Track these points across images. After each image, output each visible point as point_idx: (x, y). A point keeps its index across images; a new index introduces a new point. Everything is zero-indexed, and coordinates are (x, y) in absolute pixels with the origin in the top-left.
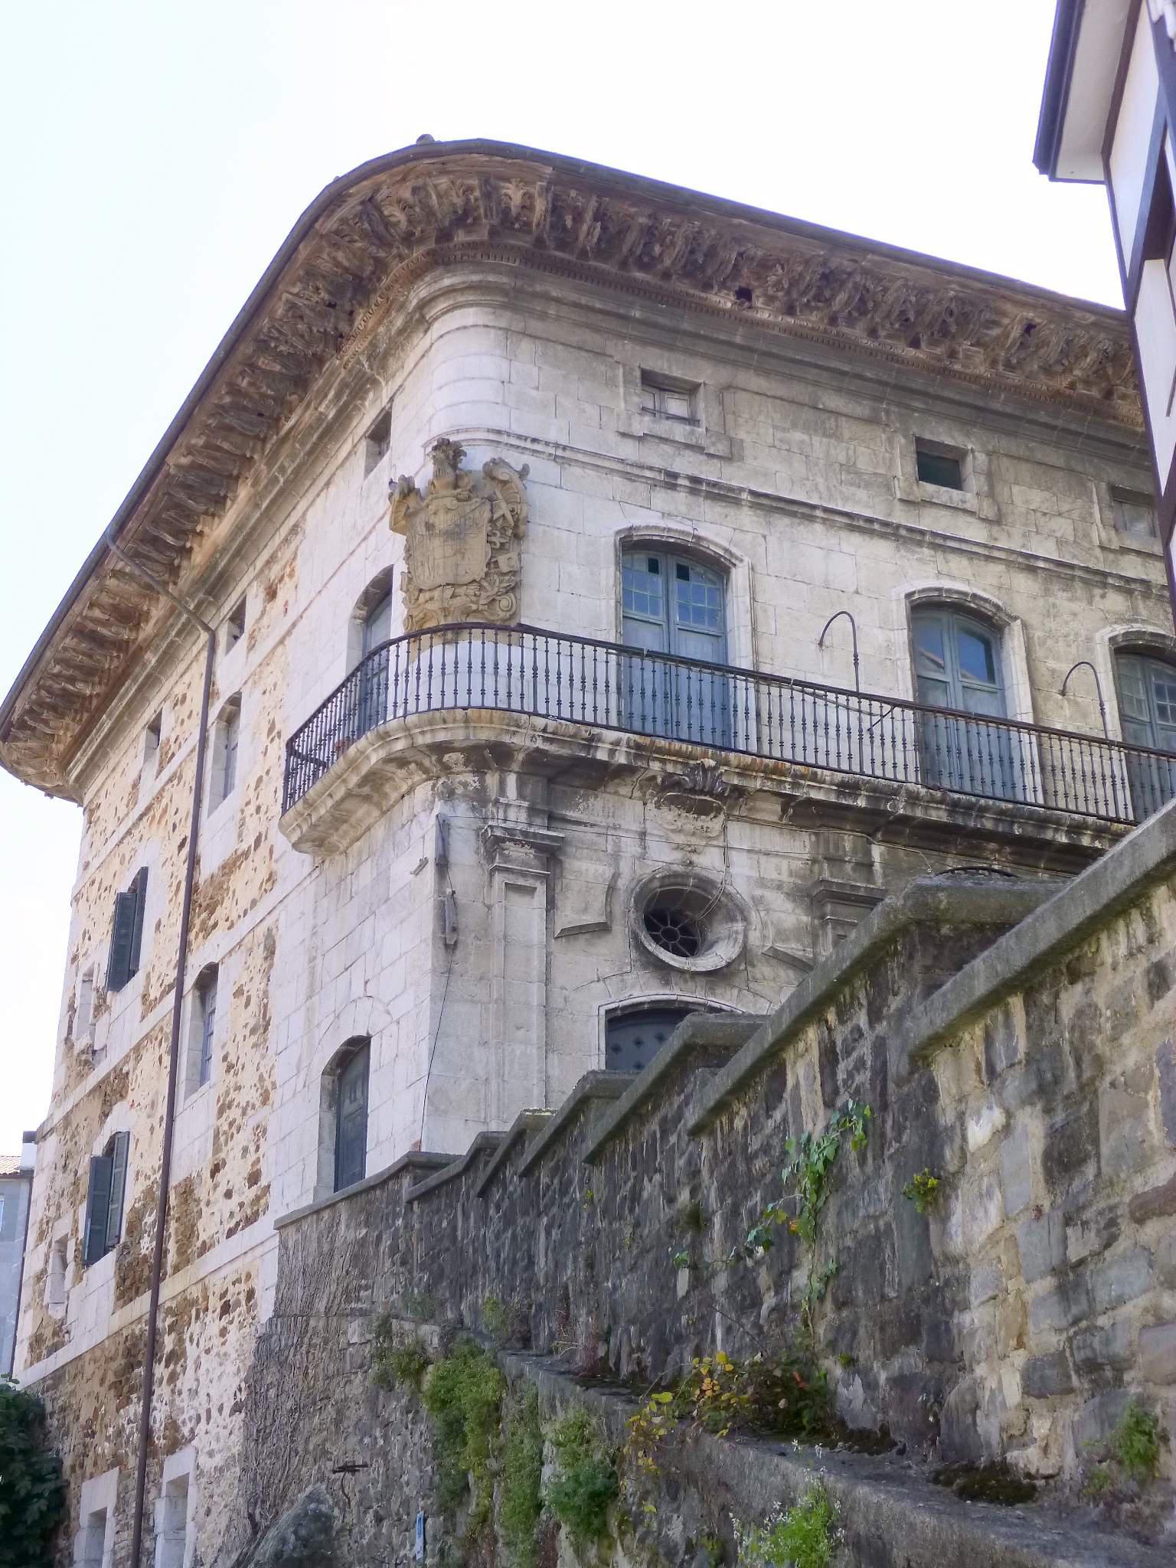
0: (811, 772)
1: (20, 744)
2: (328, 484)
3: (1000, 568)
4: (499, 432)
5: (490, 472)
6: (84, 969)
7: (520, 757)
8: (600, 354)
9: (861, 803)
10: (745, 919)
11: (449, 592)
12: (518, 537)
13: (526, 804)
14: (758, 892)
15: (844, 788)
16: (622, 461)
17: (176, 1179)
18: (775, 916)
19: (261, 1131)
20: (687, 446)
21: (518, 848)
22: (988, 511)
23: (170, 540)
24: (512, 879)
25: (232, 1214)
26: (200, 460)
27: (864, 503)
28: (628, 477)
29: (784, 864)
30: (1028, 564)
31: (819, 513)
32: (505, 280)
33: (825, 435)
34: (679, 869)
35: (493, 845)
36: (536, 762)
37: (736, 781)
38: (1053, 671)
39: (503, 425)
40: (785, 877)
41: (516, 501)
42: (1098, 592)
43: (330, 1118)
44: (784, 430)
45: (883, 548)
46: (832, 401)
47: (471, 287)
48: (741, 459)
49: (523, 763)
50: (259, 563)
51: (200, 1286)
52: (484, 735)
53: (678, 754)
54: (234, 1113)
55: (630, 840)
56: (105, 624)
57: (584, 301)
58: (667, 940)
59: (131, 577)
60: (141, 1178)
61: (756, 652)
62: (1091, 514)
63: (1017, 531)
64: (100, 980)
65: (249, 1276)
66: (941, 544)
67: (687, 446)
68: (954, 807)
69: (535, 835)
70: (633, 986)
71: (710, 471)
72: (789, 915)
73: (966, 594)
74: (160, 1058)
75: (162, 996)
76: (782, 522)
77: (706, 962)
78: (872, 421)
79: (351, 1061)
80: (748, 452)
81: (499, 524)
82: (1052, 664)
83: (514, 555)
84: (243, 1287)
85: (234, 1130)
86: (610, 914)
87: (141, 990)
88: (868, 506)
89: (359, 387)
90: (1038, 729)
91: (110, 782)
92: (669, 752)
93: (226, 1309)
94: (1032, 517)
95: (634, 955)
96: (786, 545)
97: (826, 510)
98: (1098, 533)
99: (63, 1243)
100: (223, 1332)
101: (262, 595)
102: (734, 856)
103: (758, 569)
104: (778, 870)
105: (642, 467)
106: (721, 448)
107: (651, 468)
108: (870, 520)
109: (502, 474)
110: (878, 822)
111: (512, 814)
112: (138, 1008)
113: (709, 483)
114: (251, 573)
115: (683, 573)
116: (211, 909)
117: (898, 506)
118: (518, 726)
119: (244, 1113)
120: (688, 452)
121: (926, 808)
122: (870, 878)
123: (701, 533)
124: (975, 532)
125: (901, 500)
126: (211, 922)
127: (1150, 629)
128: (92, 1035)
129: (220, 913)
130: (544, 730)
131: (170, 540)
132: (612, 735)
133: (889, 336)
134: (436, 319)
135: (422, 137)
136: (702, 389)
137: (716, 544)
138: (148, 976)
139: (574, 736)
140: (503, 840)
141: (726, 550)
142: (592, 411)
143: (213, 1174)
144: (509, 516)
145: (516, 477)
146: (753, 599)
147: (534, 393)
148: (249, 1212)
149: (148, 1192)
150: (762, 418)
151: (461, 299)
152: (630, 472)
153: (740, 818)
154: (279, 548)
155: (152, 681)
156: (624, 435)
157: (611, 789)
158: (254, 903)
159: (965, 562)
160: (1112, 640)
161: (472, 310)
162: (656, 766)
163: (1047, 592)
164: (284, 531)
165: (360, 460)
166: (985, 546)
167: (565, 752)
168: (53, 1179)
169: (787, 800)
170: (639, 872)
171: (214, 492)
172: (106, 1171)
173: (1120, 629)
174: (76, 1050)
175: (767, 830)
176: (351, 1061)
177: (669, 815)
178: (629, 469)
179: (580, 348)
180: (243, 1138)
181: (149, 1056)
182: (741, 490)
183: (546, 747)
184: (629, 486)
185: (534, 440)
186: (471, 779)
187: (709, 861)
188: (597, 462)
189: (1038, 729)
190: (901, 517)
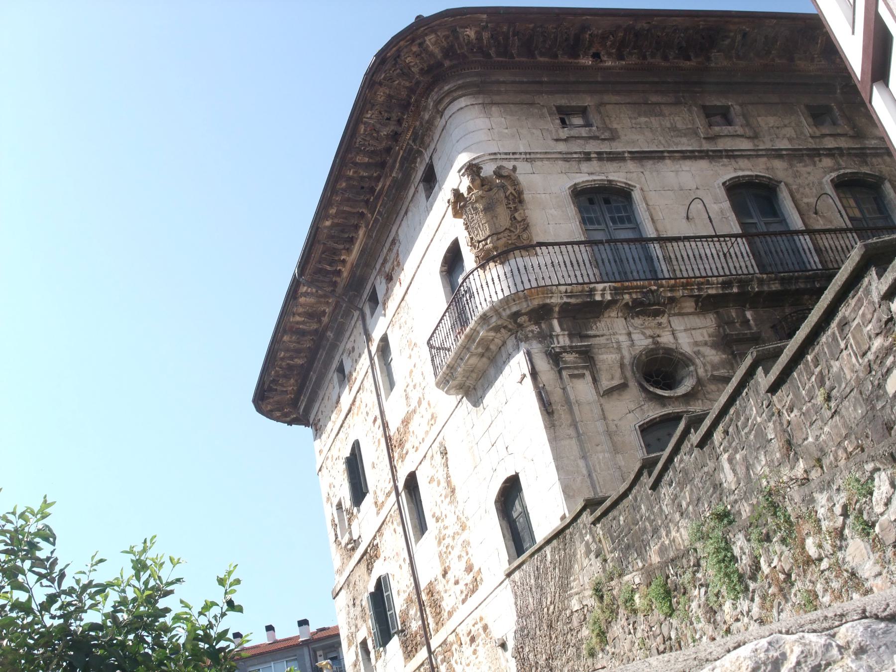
0: (706, 280)
1: (271, 400)
2: (406, 213)
3: (764, 160)
4: (495, 154)
5: (498, 173)
6: (335, 503)
7: (557, 309)
8: (532, 104)
9: (735, 290)
10: (694, 364)
11: (495, 238)
12: (521, 201)
13: (566, 333)
14: (696, 349)
15: (727, 284)
16: (560, 153)
17: (423, 585)
18: (708, 359)
19: (466, 544)
20: (590, 138)
21: (570, 355)
22: (749, 133)
23: (329, 268)
24: (571, 372)
25: (462, 592)
26: (336, 221)
27: (686, 144)
28: (566, 160)
29: (704, 331)
30: (777, 154)
31: (666, 154)
32: (475, 79)
33: (656, 116)
34: (653, 346)
35: (555, 358)
36: (565, 308)
37: (669, 295)
38: (808, 204)
39: (496, 151)
40: (707, 338)
41: (515, 183)
42: (817, 159)
43: (505, 523)
44: (635, 118)
45: (703, 164)
46: (654, 99)
47: (460, 88)
48: (619, 137)
49: (559, 312)
50: (378, 266)
51: (454, 634)
52: (536, 302)
53: (637, 287)
54: (448, 541)
55: (622, 339)
56: (303, 323)
57: (517, 79)
58: (656, 384)
59: (312, 294)
60: (402, 593)
61: (657, 230)
62: (801, 122)
63: (767, 139)
64: (347, 503)
65: (481, 619)
66: (731, 155)
67: (590, 138)
68: (783, 281)
69: (576, 346)
70: (648, 411)
71: (605, 148)
72: (713, 356)
73: (752, 176)
74: (395, 530)
75: (386, 499)
76: (649, 164)
77: (681, 390)
78: (677, 103)
79: (510, 493)
80: (621, 133)
81: (511, 197)
82: (806, 200)
83: (521, 211)
84: (480, 626)
85: (450, 549)
86: (625, 378)
87: (373, 501)
88: (689, 145)
89: (411, 156)
90: (810, 231)
91: (322, 405)
92: (632, 288)
93: (473, 640)
94: (772, 130)
95: (643, 395)
96: (655, 174)
97: (669, 152)
98: (808, 130)
99: (364, 643)
100: (475, 652)
101: (384, 281)
102: (679, 335)
103: (645, 189)
104: (702, 335)
105: (571, 153)
106: (607, 135)
107: (576, 153)
108: (692, 151)
109: (504, 173)
110: (745, 299)
111: (561, 339)
112: (375, 510)
113: (606, 153)
114: (375, 273)
115: (607, 201)
116: (401, 444)
117: (704, 141)
118: (552, 293)
119: (454, 539)
120: (591, 141)
121: (769, 285)
122: (750, 328)
123: (611, 178)
124: (745, 145)
125: (705, 138)
126: (404, 452)
127: (849, 171)
128: (350, 533)
129: (408, 446)
130: (566, 292)
131: (329, 268)
132: (600, 286)
133: (674, 58)
134: (445, 109)
135: (418, 17)
136: (589, 109)
137: (620, 182)
138: (375, 493)
139: (582, 291)
140: (561, 353)
141: (626, 183)
142: (537, 133)
143: (444, 576)
144: (513, 192)
145: (512, 173)
146: (647, 204)
147: (506, 131)
148: (471, 587)
149: (409, 601)
150: (622, 115)
151: (455, 94)
152: (566, 158)
153: (674, 315)
154: (387, 254)
155: (334, 347)
156: (557, 140)
157: (606, 315)
158: (427, 433)
159: (746, 161)
160: (832, 181)
161: (462, 99)
162: (627, 297)
163: (791, 166)
164: (387, 245)
165: (422, 194)
166: (753, 150)
167: (579, 301)
168: (349, 613)
169: (697, 298)
170: (633, 353)
171: (346, 236)
172: (380, 598)
173: (834, 175)
174: (343, 545)
175: (691, 317)
176: (510, 493)
177: (637, 321)
178: (565, 156)
179: (522, 104)
180: (455, 553)
181: (388, 531)
182: (624, 152)
183: (569, 300)
184: (567, 165)
185: (514, 153)
186: (535, 328)
187: (666, 339)
188: (546, 156)
189: (810, 231)
190: (706, 146)
